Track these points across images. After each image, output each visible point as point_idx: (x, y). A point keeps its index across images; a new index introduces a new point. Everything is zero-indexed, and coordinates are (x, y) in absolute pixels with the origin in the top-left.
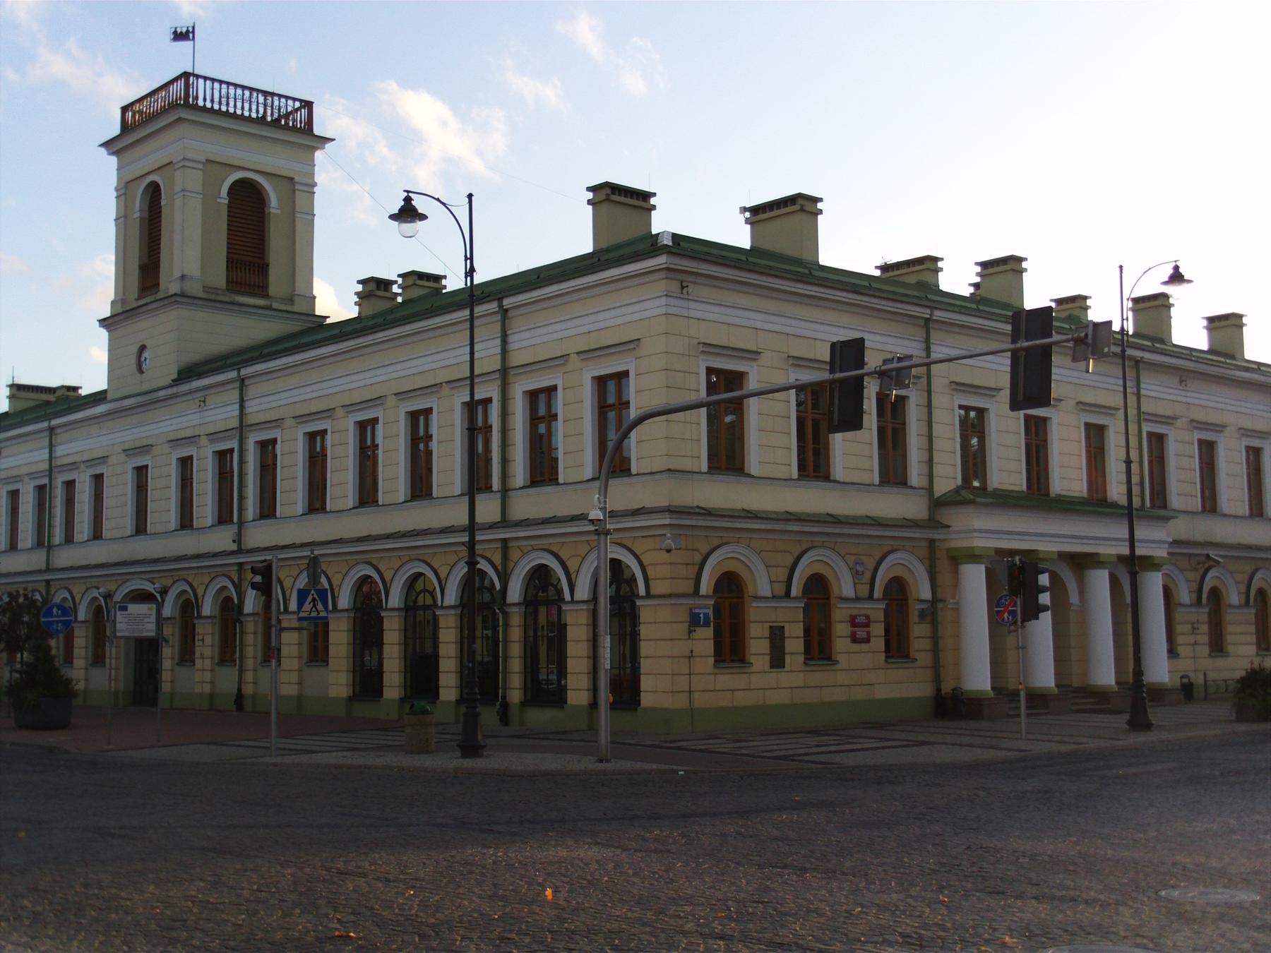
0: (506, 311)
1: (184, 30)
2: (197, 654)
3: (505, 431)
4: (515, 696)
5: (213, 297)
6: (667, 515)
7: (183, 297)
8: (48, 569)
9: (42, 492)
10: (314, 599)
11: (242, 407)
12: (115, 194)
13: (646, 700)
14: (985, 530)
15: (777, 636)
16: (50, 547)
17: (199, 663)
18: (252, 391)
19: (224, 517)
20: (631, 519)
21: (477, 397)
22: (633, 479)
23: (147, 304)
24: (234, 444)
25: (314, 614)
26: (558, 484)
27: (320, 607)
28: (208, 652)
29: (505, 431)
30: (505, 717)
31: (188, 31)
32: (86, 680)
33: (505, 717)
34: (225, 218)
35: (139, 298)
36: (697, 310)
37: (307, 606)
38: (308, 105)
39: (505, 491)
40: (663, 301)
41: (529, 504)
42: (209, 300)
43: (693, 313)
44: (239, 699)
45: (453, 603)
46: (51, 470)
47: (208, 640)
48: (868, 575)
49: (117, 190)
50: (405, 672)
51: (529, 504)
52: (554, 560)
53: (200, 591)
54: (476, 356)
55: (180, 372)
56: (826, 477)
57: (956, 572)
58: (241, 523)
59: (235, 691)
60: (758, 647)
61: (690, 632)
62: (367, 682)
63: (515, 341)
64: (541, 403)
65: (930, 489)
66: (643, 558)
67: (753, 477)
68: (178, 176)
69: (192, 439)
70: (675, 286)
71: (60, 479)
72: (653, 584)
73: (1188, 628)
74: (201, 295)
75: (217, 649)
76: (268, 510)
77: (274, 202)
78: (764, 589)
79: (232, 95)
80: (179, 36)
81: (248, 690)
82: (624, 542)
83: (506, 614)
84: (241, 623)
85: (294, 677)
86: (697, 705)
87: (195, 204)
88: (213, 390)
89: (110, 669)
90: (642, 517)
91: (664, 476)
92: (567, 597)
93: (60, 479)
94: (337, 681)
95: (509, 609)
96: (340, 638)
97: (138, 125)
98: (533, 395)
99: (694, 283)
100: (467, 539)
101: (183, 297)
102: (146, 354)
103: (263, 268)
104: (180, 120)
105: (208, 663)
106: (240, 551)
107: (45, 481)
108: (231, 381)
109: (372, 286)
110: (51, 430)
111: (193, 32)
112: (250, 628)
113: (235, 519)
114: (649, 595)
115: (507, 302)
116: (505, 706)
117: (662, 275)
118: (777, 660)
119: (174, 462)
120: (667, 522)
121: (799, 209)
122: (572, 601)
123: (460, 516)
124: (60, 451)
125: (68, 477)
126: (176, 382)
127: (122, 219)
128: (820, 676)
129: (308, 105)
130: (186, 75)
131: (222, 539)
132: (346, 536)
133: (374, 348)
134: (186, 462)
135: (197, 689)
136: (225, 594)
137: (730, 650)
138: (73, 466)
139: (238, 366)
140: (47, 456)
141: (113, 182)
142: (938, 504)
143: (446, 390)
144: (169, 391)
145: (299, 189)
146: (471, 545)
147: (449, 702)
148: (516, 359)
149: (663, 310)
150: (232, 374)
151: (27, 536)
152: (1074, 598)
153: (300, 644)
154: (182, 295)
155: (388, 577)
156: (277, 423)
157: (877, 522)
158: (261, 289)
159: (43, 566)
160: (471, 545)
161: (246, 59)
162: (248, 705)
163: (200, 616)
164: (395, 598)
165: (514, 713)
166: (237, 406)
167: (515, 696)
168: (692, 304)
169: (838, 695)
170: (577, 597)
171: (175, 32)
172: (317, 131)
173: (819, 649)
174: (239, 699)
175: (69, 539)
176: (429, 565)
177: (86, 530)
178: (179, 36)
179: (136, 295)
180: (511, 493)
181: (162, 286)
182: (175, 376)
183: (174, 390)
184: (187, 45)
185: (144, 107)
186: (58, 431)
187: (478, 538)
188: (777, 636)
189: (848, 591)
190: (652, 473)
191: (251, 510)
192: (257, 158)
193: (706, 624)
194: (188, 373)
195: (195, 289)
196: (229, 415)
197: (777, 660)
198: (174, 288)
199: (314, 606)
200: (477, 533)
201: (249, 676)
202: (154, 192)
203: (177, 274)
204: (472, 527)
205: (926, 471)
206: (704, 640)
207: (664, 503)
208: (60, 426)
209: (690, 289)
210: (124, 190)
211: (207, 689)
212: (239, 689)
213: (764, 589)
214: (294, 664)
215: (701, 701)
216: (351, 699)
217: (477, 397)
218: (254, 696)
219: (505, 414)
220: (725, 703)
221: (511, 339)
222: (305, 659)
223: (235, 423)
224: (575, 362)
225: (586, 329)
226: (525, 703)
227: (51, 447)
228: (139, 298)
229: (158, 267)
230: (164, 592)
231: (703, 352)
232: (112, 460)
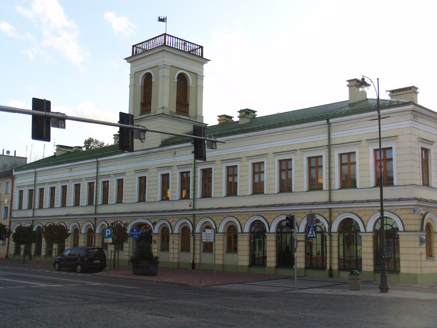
0: (330, 124)
1: (163, 18)
2: (66, 245)
3: (194, 181)
4: (33, 253)
5: (172, 115)
6: (416, 201)
7: (163, 115)
8: (96, 214)
9: (31, 192)
10: (312, 230)
11: (97, 170)
12: (129, 77)
13: (403, 270)
16: (96, 205)
17: (171, 251)
18: (100, 165)
19: (90, 203)
20: (398, 202)
21: (382, 147)
22: (238, 197)
23: (147, 117)
24: (191, 170)
25: (312, 236)
26: (394, 186)
27: (314, 233)
28: (176, 247)
29: (194, 181)
30: (30, 259)
31: (164, 19)
32: (200, 259)
33: (30, 259)
34: (176, 87)
35: (141, 115)
36: (420, 126)
39: (194, 199)
40: (410, 122)
41: (203, 204)
42: (171, 116)
43: (419, 128)
44: (193, 264)
45: (274, 232)
47: (176, 242)
49: (130, 75)
50: (250, 256)
51: (203, 204)
52: (261, 218)
53: (81, 225)
54: (381, 130)
55: (162, 142)
58: (194, 199)
59: (192, 262)
61: (420, 245)
62: (257, 260)
63: (333, 135)
64: (106, 185)
66: (362, 218)
67: (433, 188)
68: (161, 71)
70: (412, 116)
71: (38, 188)
72: (405, 227)
74: (169, 114)
75: (72, 243)
76: (105, 201)
79: (181, 43)
80: (162, 20)
81: (197, 261)
82: (353, 212)
83: (330, 236)
84: (95, 236)
85: (221, 257)
86: (423, 272)
87: (167, 81)
88: (178, 150)
89: (194, 254)
90: (401, 202)
91: (412, 186)
92: (268, 231)
93: (38, 188)
94: (243, 258)
95: (332, 234)
96: (243, 244)
97: (138, 54)
98: (104, 182)
99: (420, 117)
100: (380, 205)
101: (163, 115)
104: (164, 50)
105: (176, 251)
106: (96, 214)
109: (244, 113)
110: (36, 172)
111: (166, 19)
112: (97, 237)
113: (94, 204)
114: (242, 232)
115: (331, 121)
116: (31, 256)
117: (410, 112)
119: (60, 187)
120: (416, 203)
121: (358, 84)
122: (269, 233)
123: (376, 194)
124: (101, 170)
125: (41, 187)
126: (161, 146)
127: (133, 86)
130: (165, 35)
132: (222, 206)
133: (153, 154)
135: (171, 260)
136: (75, 227)
139: (97, 157)
140: (34, 180)
141: (129, 72)
143: (58, 183)
144: (158, 149)
146: (382, 206)
147: (369, 272)
148: (333, 142)
149: (410, 125)
150: (95, 160)
153: (84, 242)
154: (163, 114)
156: (109, 176)
158: (186, 113)
159: (94, 213)
160: (382, 206)
161: (183, 30)
162: (197, 267)
163: (80, 233)
165: (32, 257)
166: (96, 169)
167: (33, 253)
168: (419, 124)
170: (271, 231)
171: (159, 18)
174: (193, 264)
176: (212, 219)
177: (86, 202)
178: (162, 20)
179: (139, 114)
180: (332, 191)
181: (152, 110)
182: (160, 144)
183: (161, 149)
184: (163, 23)
185: (144, 46)
186: (100, 163)
187: (384, 205)
190: (404, 185)
191: (100, 201)
192: (186, 66)
194: (165, 143)
195: (167, 112)
196: (31, 181)
198: (159, 112)
200: (384, 202)
201: (197, 256)
203: (160, 106)
204: (382, 200)
205: (332, 169)
207: (66, 214)
208: (102, 161)
209: (418, 118)
210: (134, 76)
211: (176, 260)
212: (193, 261)
214: (221, 252)
216: (14, 254)
217: (382, 147)
218: (200, 263)
219: (195, 177)
221: (332, 134)
222: (225, 250)
223: (326, 143)
224: (364, 143)
225: (371, 131)
226: (339, 269)
227: (97, 168)
228: (141, 115)
229: (151, 103)
230: (154, 224)
231: (421, 141)
232: (127, 174)
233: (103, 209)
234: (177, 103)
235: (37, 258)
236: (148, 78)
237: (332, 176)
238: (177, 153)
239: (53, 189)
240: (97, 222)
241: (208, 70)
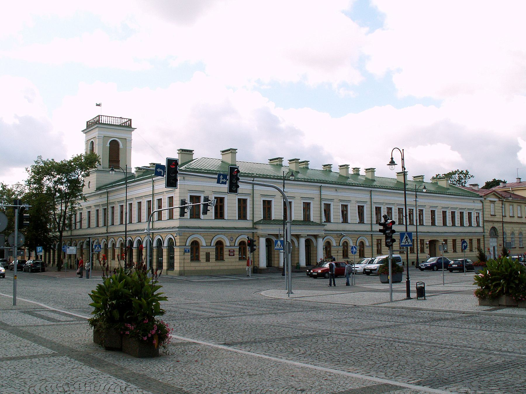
10: (406, 237)
14: (265, 230)
15: (208, 255)
25: (407, 244)
27: (409, 240)
37: (97, 248)
38: (130, 120)
39: (126, 224)
46: (153, 194)
48: (234, 241)
56: (224, 219)
57: (259, 239)
58: (126, 224)
60: (203, 257)
63: (156, 187)
65: (253, 220)
69: (98, 206)
71: (157, 198)
73: (339, 252)
76: (160, 218)
77: (121, 146)
78: (204, 244)
80: (98, 105)
102: (90, 184)
103: (118, 162)
106: (107, 233)
107: (150, 199)
108: (105, 192)
109: (137, 169)
118: (208, 259)
128: (220, 263)
129: (130, 120)
130: (99, 116)
131: (104, 230)
134: (98, 210)
137: (195, 258)
138: (113, 203)
142: (254, 224)
145: (127, 141)
146: (126, 234)
148: (156, 192)
151: (101, 223)
152: (296, 245)
155: (164, 238)
157: (235, 228)
160: (126, 234)
161: (113, 111)
164: (166, 244)
169: (225, 268)
172: (133, 127)
173: (220, 257)
175: (131, 222)
178: (98, 105)
188: (208, 255)
189: (228, 244)
192: (116, 135)
193: (188, 252)
197: (208, 259)
199: (407, 240)
202: (92, 143)
204: (126, 231)
206: (188, 255)
213: (204, 244)
215: (186, 268)
220: (194, 269)
233: (158, 225)
234: (110, 161)
235: (170, 273)
236: (92, 143)
237: (251, 202)
238: (186, 178)
239: (140, 203)
240: (155, 236)
241: (134, 135)
